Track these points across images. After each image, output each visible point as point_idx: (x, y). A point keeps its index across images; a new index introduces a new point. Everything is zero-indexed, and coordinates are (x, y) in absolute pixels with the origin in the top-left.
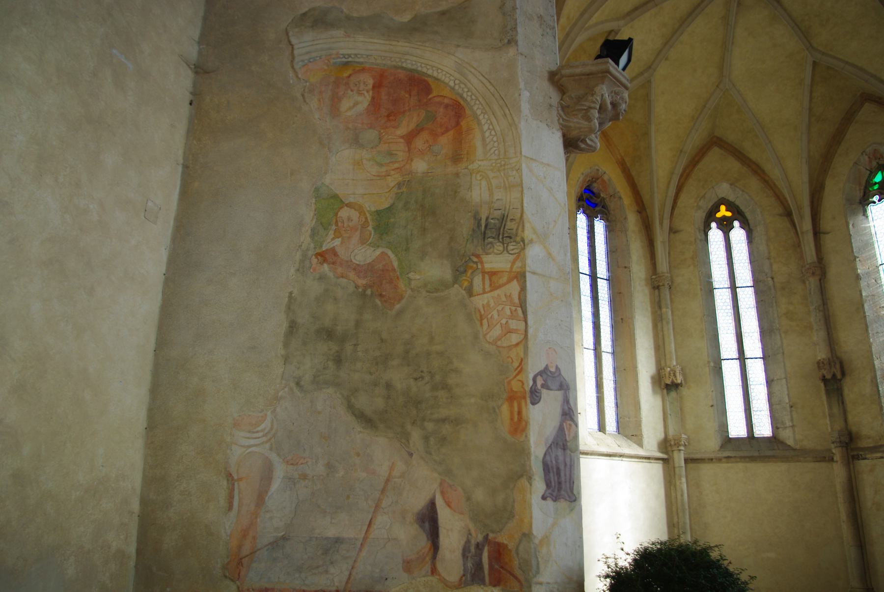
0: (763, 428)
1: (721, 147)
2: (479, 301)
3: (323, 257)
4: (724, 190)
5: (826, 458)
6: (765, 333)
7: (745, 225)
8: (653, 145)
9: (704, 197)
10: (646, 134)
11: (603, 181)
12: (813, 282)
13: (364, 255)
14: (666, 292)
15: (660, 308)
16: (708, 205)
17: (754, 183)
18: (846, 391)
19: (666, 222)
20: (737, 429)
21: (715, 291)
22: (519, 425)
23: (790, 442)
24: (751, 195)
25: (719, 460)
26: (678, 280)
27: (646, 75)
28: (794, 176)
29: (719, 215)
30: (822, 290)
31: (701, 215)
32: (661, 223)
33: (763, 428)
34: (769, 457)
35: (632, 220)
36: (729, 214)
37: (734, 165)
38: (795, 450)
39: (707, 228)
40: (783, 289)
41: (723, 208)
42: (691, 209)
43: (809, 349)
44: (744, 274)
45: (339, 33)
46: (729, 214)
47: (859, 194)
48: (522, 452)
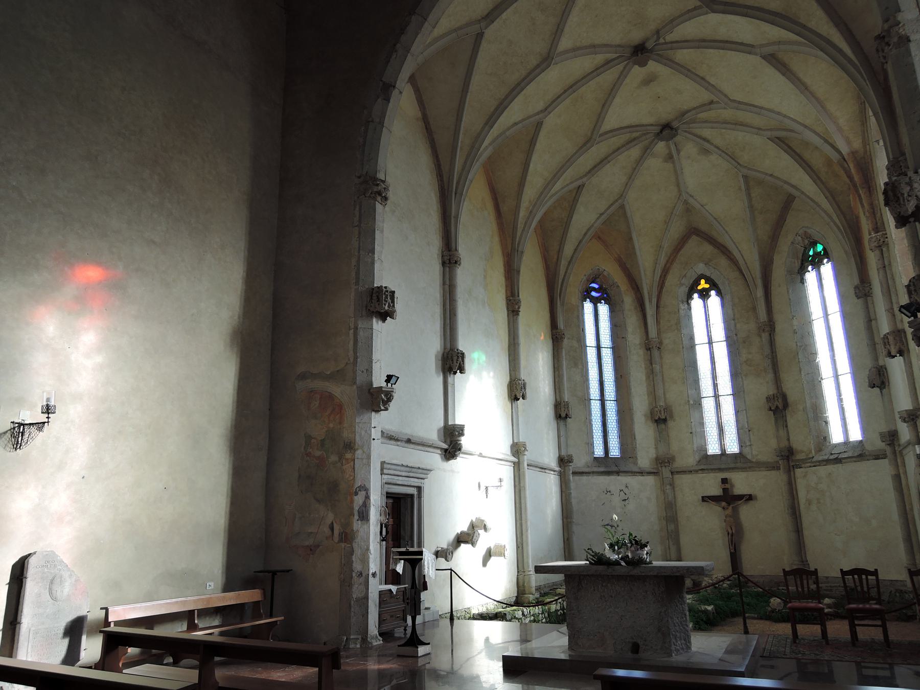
0: (733, 447)
1: (698, 235)
2: (344, 467)
3: (307, 455)
4: (701, 268)
5: (773, 467)
6: (735, 375)
7: (719, 293)
8: (637, 246)
9: (685, 276)
10: (631, 239)
11: (604, 276)
12: (765, 336)
13: (318, 453)
14: (656, 353)
15: (651, 364)
16: (688, 282)
17: (723, 262)
18: (788, 418)
19: (654, 300)
20: (713, 448)
21: (697, 347)
22: (352, 501)
23: (749, 457)
24: (722, 270)
25: (696, 471)
26: (666, 342)
27: (620, 201)
28: (750, 256)
29: (700, 288)
30: (772, 342)
31: (684, 290)
32: (650, 301)
33: (733, 447)
34: (733, 468)
35: (628, 301)
36: (707, 286)
37: (708, 248)
38: (751, 462)
39: (689, 297)
40: (744, 342)
41: (703, 281)
42: (675, 284)
43: (762, 388)
44: (719, 333)
45: (309, 381)
46: (707, 286)
47: (797, 264)
48: (353, 509)
